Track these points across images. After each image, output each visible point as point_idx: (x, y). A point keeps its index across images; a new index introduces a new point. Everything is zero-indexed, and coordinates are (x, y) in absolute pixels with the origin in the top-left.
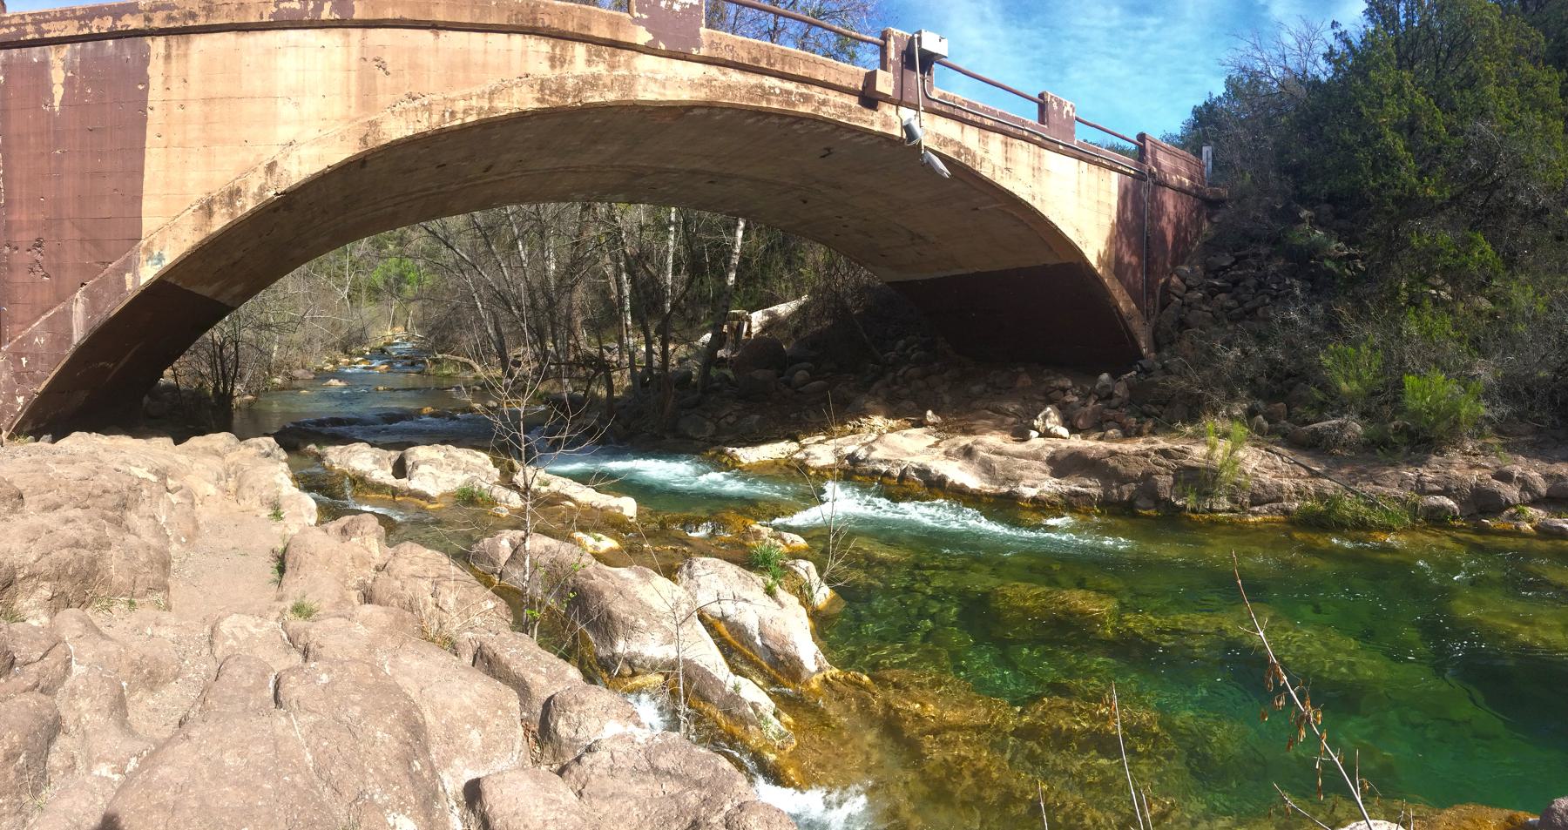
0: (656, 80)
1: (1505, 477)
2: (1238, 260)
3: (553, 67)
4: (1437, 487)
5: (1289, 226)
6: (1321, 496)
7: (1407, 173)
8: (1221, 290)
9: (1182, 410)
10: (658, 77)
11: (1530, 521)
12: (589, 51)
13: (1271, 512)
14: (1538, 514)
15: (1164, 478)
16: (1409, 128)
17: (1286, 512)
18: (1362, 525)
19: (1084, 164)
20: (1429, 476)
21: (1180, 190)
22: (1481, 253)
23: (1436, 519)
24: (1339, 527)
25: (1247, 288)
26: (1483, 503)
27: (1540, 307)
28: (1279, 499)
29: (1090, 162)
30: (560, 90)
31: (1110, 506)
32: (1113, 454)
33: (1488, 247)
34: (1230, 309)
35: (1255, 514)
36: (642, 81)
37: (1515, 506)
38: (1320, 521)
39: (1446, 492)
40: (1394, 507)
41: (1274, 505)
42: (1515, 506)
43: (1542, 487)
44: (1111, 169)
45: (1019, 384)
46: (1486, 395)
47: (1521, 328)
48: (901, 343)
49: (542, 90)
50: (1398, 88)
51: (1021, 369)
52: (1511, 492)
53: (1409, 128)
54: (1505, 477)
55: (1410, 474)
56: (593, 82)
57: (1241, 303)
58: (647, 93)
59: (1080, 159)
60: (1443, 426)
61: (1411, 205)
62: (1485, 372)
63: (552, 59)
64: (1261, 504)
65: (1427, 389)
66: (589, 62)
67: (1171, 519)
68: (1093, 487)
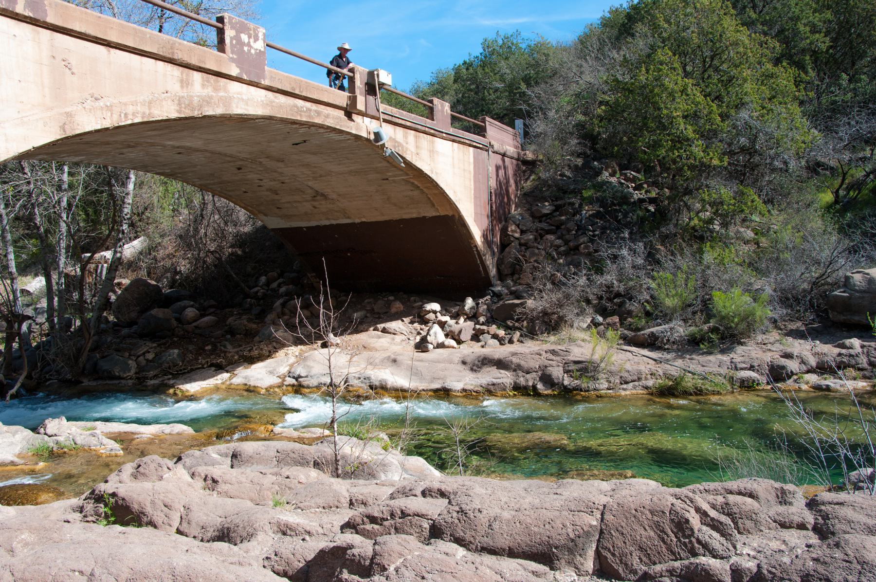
0: (242, 99)
1: (788, 356)
2: (557, 208)
3: (182, 87)
4: (744, 366)
5: (603, 187)
6: (668, 377)
7: (697, 149)
8: (548, 232)
9: (550, 323)
10: (244, 97)
11: (807, 383)
12: (203, 78)
13: (635, 387)
14: (813, 378)
15: (556, 369)
16: (692, 117)
17: (647, 388)
18: (699, 392)
19: (456, 144)
20: (738, 359)
21: (512, 158)
22: (753, 201)
23: (747, 386)
24: (686, 394)
25: (569, 231)
26: (777, 374)
27: (798, 240)
28: (639, 379)
29: (459, 142)
30: (190, 105)
31: (520, 390)
32: (514, 354)
33: (756, 198)
34: (559, 247)
35: (624, 389)
36: (236, 101)
37: (796, 374)
38: (669, 391)
39: (752, 368)
40: (719, 380)
41: (636, 383)
42: (796, 374)
43: (813, 362)
44: (470, 145)
45: (393, 310)
46: (770, 302)
47: (787, 255)
48: (263, 279)
49: (179, 104)
50: (683, 91)
51: (392, 298)
52: (793, 365)
53: (692, 117)
54: (788, 356)
55: (725, 358)
56: (207, 101)
57: (566, 242)
58: (238, 109)
59: (453, 141)
60: (743, 326)
61: (703, 169)
62: (767, 286)
63: (182, 81)
64: (626, 383)
65: (730, 301)
66: (203, 86)
67: (568, 396)
68: (506, 378)
